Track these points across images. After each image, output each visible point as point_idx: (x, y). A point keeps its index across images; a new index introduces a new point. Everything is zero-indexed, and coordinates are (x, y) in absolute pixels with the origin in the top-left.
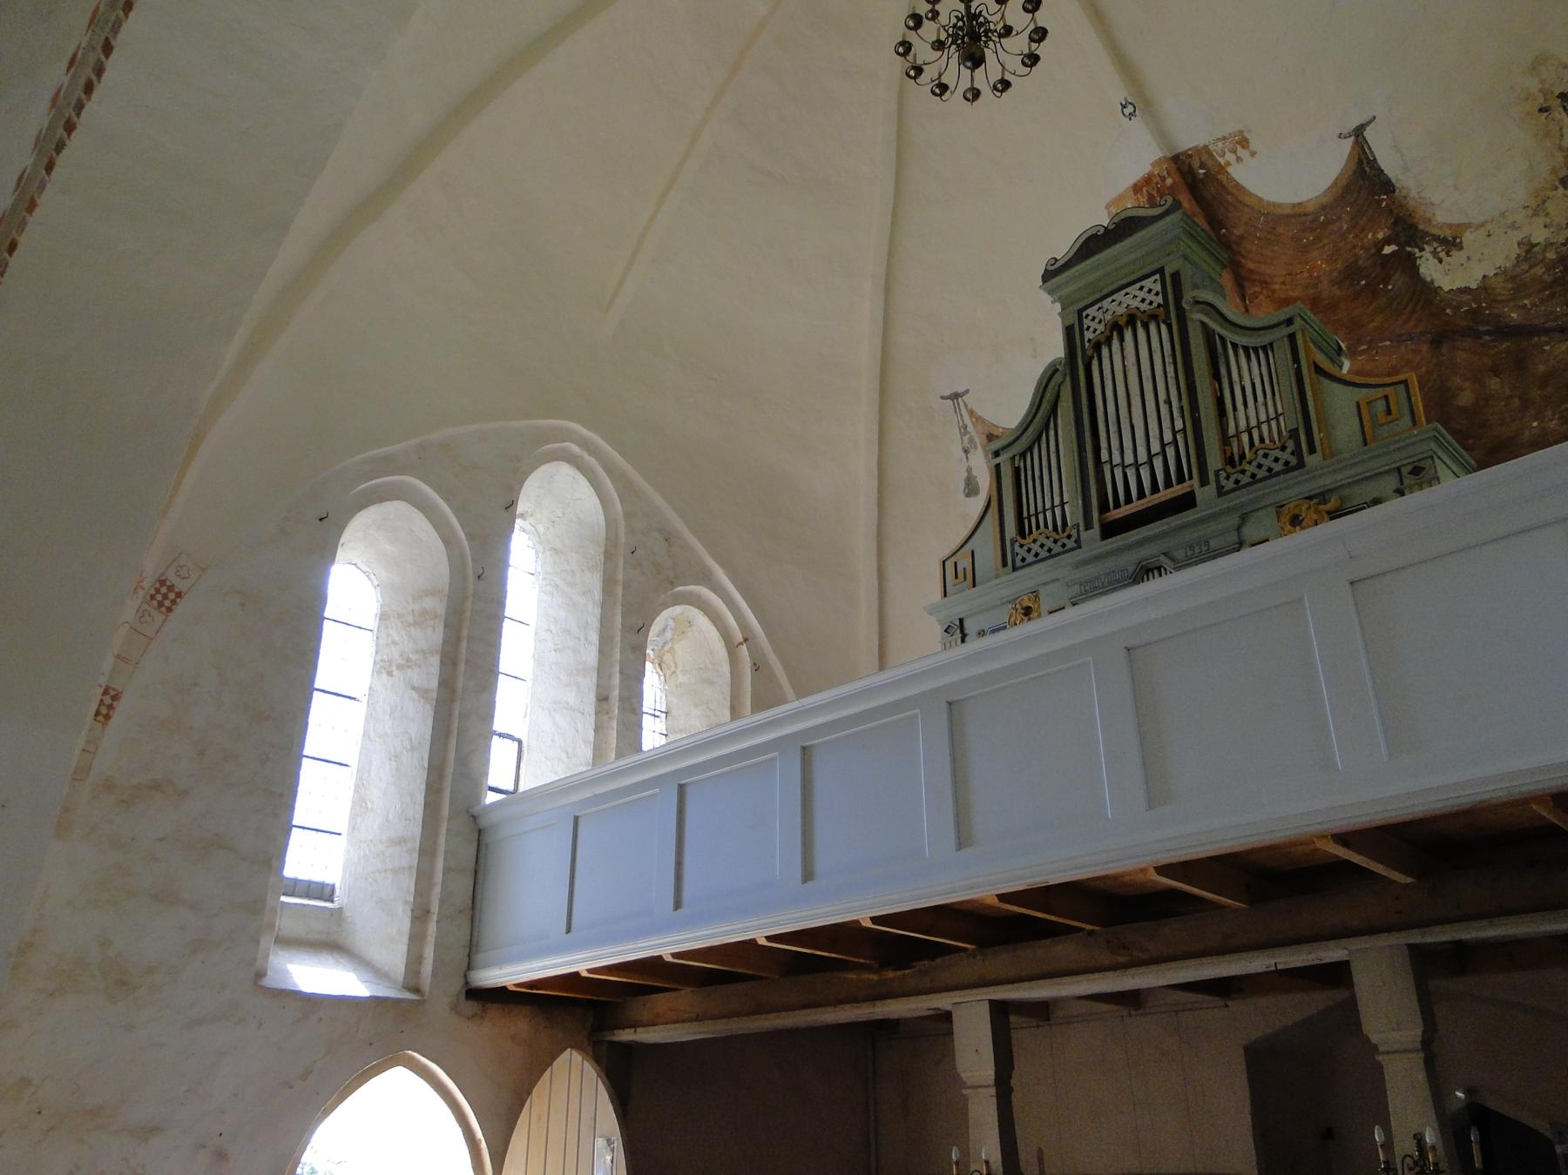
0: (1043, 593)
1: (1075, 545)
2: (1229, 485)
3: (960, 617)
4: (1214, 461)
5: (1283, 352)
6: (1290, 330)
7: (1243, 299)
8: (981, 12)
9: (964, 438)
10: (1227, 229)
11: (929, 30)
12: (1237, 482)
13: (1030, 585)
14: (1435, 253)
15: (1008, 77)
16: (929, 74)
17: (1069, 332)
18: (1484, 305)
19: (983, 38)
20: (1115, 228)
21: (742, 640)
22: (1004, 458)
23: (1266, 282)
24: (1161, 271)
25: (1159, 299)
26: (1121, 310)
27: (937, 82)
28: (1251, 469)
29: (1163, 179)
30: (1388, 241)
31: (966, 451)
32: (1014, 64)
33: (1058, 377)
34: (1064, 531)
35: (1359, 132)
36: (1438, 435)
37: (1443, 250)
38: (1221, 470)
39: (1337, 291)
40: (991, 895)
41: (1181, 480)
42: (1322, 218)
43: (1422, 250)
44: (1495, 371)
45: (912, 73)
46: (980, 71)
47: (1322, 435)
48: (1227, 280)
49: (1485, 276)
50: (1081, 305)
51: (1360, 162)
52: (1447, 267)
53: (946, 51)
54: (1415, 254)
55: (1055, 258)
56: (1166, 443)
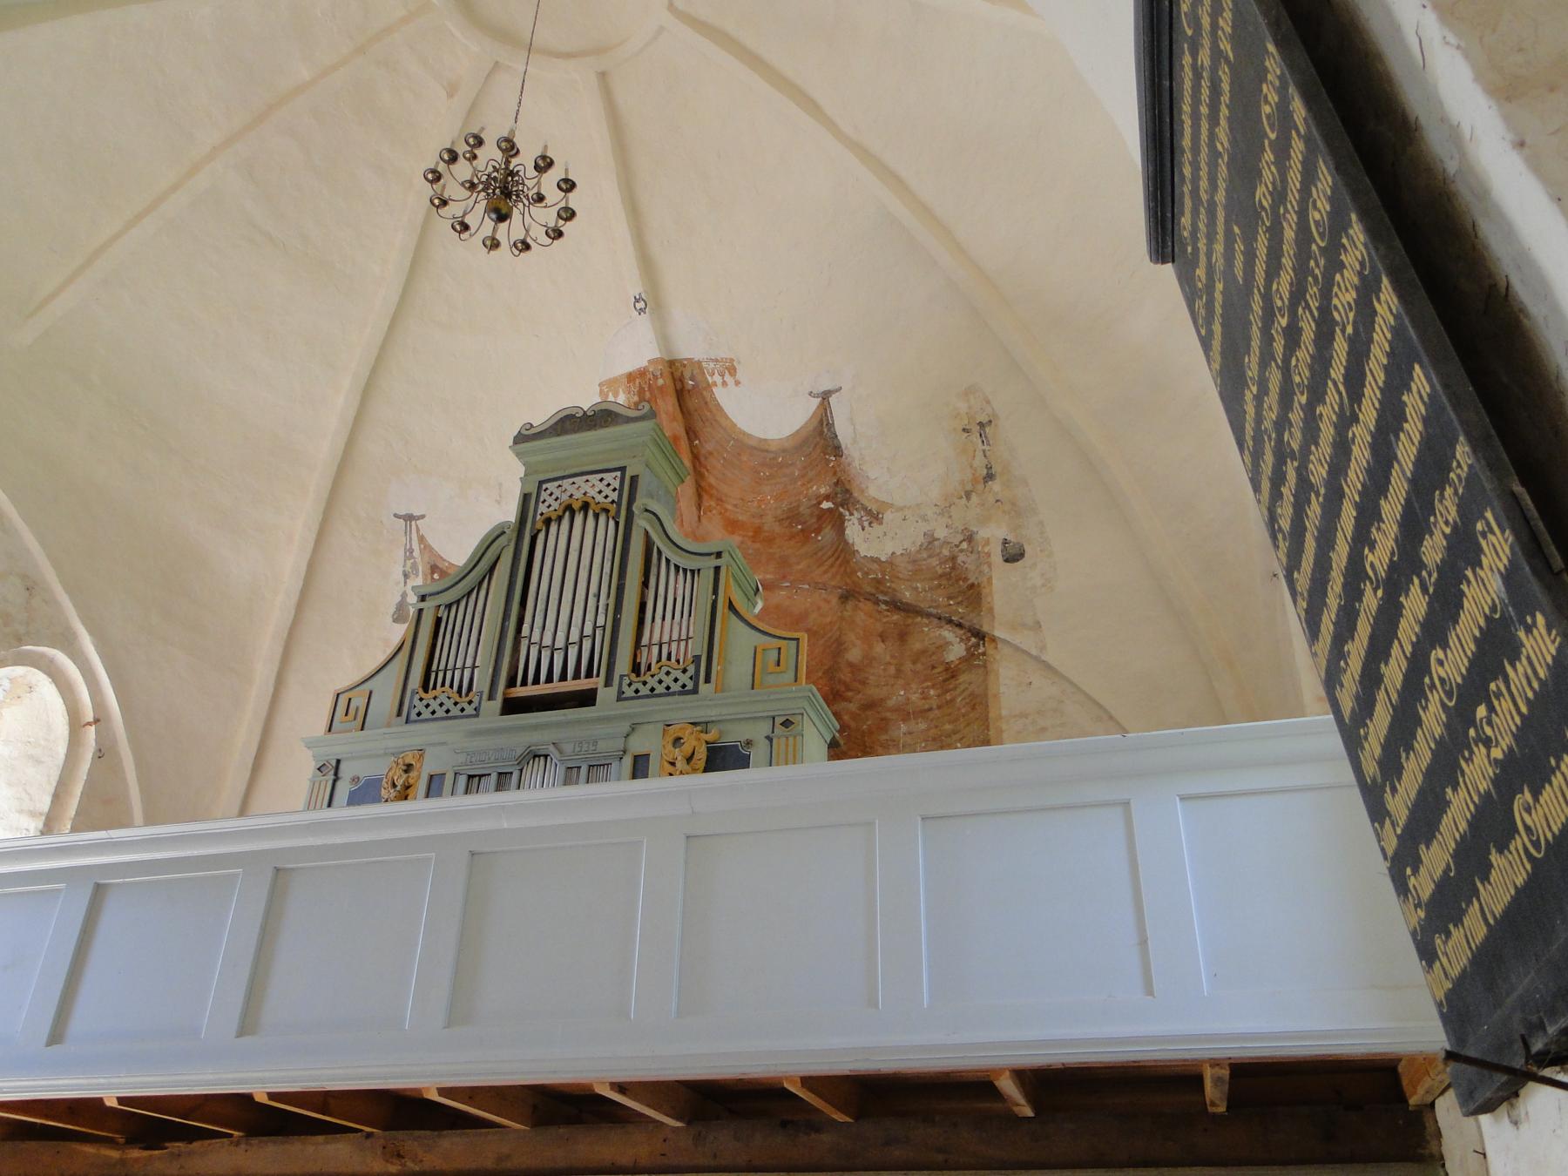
0: (429, 752)
1: (475, 712)
2: (629, 692)
3: (339, 758)
4: (623, 665)
5: (707, 577)
6: (718, 562)
7: (699, 507)
8: (518, 171)
9: (407, 561)
10: (700, 441)
11: (463, 170)
12: (637, 691)
13: (417, 742)
14: (860, 520)
15: (529, 240)
16: (454, 210)
17: (526, 498)
18: (887, 577)
19: (514, 197)
20: (593, 415)
21: (91, 720)
22: (429, 605)
23: (721, 500)
24: (623, 469)
25: (614, 496)
26: (578, 495)
27: (460, 219)
28: (652, 682)
29: (656, 377)
30: (827, 498)
31: (406, 576)
32: (538, 233)
33: (502, 540)
34: (467, 695)
35: (825, 396)
36: (811, 696)
37: (866, 520)
38: (627, 675)
39: (777, 529)
40: (263, 1092)
41: (589, 675)
42: (780, 459)
43: (851, 514)
44: (883, 637)
45: (437, 202)
46: (503, 226)
47: (719, 668)
48: (687, 490)
49: (893, 553)
50: (542, 478)
51: (821, 422)
52: (867, 536)
53: (475, 194)
54: (844, 516)
55: (531, 425)
56: (585, 634)
